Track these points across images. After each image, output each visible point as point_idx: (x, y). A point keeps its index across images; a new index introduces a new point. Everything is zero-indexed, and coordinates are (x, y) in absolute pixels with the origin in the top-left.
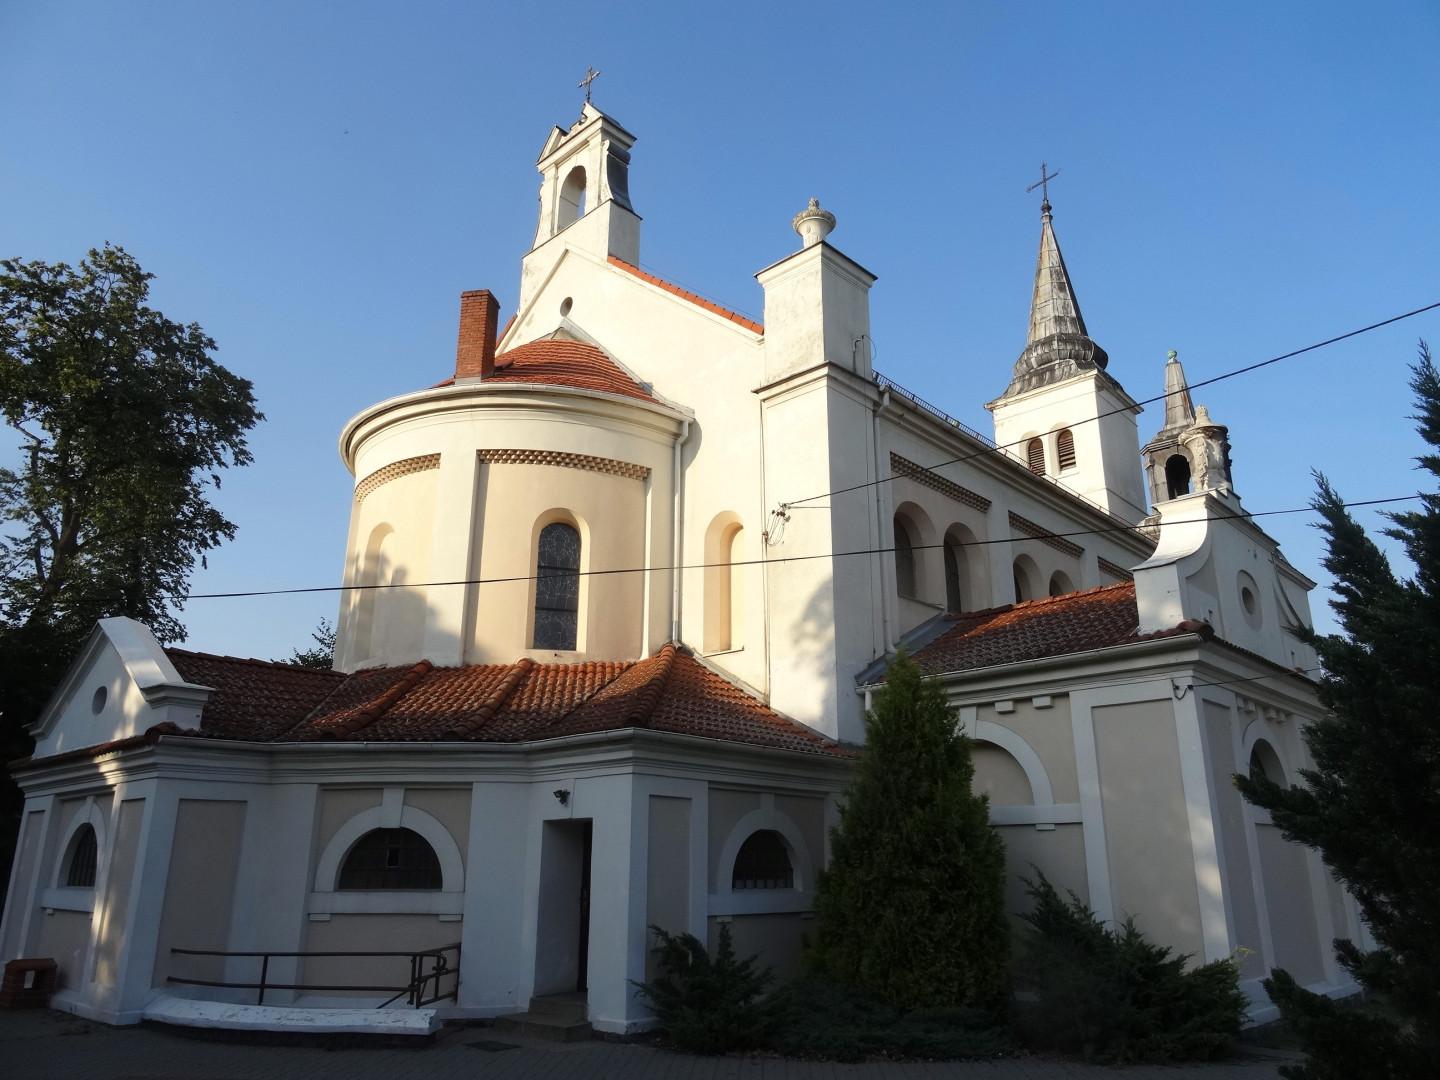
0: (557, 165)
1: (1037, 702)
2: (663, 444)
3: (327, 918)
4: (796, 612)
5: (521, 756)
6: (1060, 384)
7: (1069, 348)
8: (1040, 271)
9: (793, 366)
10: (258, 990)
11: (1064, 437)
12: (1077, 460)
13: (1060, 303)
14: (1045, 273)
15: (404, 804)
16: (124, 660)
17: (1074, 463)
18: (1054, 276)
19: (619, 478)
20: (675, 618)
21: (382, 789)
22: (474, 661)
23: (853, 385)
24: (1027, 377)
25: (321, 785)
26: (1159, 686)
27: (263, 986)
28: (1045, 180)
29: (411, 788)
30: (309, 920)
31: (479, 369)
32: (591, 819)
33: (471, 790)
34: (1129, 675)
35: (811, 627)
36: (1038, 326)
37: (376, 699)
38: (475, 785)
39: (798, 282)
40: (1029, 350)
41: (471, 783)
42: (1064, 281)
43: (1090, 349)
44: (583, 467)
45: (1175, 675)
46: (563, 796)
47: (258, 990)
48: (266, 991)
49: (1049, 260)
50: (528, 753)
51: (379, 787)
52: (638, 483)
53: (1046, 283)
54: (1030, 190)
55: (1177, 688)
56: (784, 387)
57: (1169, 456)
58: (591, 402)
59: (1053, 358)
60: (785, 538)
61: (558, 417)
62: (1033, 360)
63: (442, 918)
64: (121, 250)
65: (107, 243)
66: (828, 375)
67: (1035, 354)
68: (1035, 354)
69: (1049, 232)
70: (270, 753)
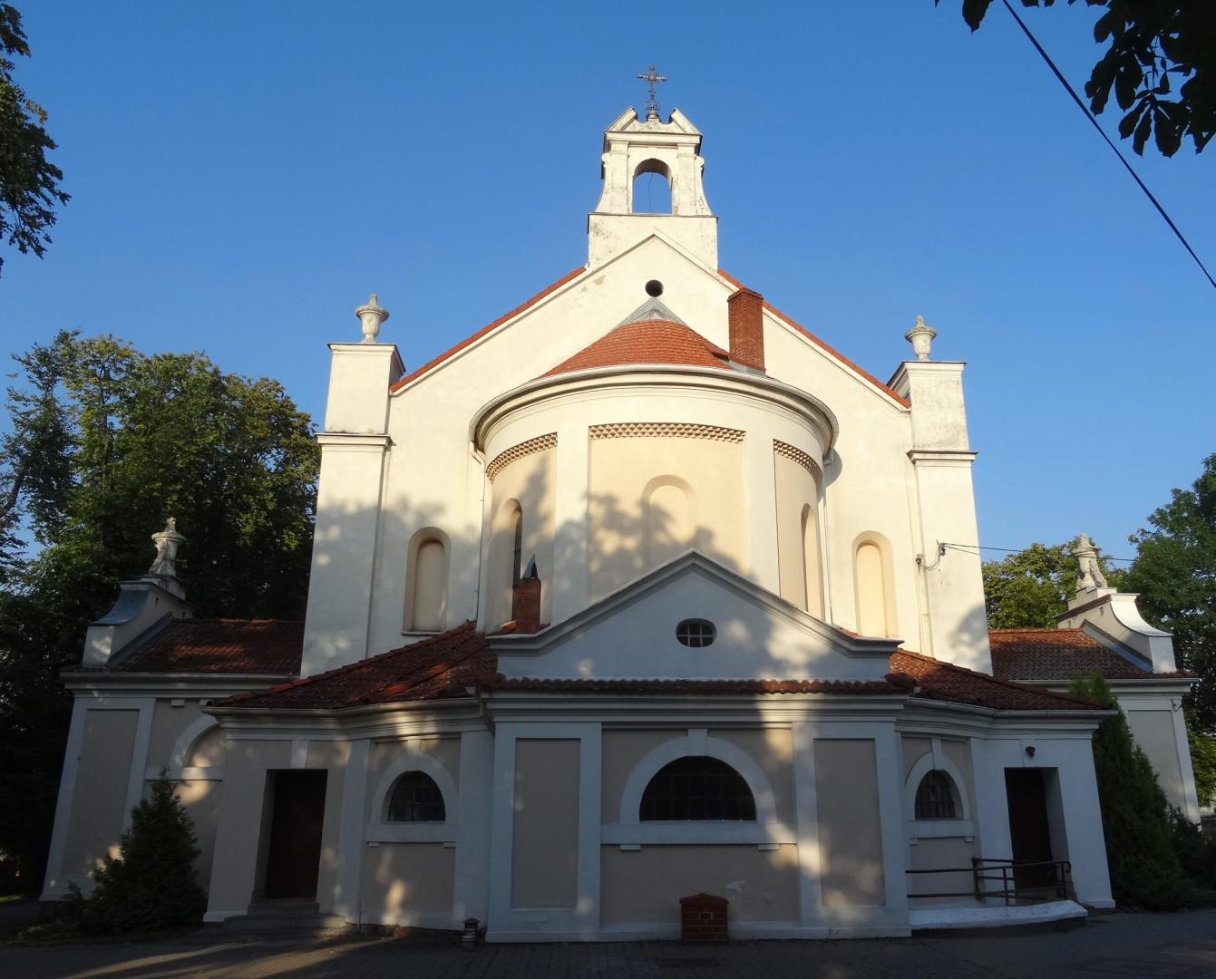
1: (174, 703)
3: (638, 848)
4: (951, 624)
5: (990, 719)
9: (941, 443)
16: (1095, 599)
21: (686, 730)
26: (1163, 703)
32: (270, 772)
33: (460, 739)
35: (965, 637)
37: (195, 645)
39: (941, 382)
41: (459, 733)
45: (1173, 698)
46: (1030, 751)
50: (994, 717)
55: (1174, 705)
56: (937, 456)
60: (940, 566)
63: (623, 848)
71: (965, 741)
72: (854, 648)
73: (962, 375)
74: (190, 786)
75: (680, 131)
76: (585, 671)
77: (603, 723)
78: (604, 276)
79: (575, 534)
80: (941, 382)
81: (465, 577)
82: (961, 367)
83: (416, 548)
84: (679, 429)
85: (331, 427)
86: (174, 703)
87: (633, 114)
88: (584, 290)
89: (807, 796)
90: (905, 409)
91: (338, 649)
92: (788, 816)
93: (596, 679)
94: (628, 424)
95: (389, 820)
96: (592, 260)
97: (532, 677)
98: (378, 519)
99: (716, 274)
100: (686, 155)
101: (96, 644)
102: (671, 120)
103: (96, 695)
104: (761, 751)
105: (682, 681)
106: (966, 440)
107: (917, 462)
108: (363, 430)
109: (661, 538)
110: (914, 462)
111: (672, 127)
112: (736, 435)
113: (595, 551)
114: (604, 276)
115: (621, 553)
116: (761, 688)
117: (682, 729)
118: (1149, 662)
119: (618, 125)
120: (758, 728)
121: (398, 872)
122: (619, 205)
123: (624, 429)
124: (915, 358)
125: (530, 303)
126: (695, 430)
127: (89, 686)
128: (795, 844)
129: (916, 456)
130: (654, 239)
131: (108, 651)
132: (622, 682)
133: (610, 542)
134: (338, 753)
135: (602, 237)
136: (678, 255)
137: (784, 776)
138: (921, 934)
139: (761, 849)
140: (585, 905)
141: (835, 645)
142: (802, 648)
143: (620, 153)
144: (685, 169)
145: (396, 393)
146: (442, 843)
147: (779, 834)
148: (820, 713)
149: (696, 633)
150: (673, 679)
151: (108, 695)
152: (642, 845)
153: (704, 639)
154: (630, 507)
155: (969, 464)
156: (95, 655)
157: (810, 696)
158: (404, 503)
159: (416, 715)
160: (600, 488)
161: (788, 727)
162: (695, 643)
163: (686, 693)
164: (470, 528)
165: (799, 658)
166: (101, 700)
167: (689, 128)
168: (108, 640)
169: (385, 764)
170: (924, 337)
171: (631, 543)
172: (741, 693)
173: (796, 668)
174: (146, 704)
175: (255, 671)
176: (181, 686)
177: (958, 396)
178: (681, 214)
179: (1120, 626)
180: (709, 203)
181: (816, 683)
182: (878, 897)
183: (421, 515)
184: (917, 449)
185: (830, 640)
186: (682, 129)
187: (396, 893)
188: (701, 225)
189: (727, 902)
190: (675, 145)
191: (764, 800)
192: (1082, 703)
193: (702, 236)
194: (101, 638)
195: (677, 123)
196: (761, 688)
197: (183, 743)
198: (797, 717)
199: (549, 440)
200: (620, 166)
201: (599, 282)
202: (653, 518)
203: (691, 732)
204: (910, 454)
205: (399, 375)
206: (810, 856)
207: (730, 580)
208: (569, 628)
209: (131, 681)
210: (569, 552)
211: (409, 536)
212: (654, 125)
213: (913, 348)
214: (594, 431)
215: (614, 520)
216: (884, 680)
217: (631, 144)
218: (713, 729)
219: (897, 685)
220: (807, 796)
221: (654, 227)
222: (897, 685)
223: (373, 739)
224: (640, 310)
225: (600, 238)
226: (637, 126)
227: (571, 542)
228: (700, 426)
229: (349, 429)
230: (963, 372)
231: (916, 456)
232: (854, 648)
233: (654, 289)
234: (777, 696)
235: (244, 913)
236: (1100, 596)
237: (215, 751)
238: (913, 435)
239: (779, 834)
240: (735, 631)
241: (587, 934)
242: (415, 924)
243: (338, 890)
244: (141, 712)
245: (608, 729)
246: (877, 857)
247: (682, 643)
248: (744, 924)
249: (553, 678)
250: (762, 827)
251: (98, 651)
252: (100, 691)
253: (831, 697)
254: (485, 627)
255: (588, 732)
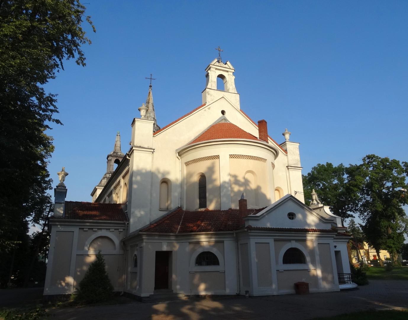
3: (283, 271)
9: (294, 164)
33: (224, 242)
56: (294, 168)
63: (280, 271)
71: (223, 242)
72: (325, 221)
73: (299, 146)
74: (90, 257)
75: (228, 67)
76: (268, 225)
77: (274, 239)
78: (210, 107)
79: (226, 185)
80: (294, 148)
81: (175, 194)
82: (298, 144)
83: (161, 183)
84: (253, 158)
85: (136, 145)
86: (85, 230)
87: (217, 60)
88: (205, 110)
89: (317, 258)
90: (286, 154)
91: (141, 215)
92: (314, 263)
93: (270, 227)
94: (240, 155)
95: (196, 265)
96: (207, 102)
97: (258, 227)
98: (151, 175)
99: (239, 111)
100: (231, 75)
101: (58, 210)
102: (226, 64)
103: (59, 226)
104: (306, 246)
105: (290, 228)
106: (300, 164)
107: (289, 169)
108: (146, 146)
109: (248, 188)
110: (288, 169)
111: (226, 66)
112: (265, 160)
113: (232, 191)
114: (210, 107)
115: (239, 191)
116: (307, 231)
117: (289, 240)
118: (336, 224)
119: (213, 63)
120: (305, 240)
121: (202, 280)
122: (214, 87)
123: (239, 156)
124: (140, 117)
125: (191, 113)
126: (256, 158)
127: (57, 223)
128: (315, 269)
129: (289, 167)
130: (223, 98)
131: (62, 212)
132: (278, 228)
133: (236, 188)
134: (174, 246)
135: (210, 96)
136: (229, 104)
137: (312, 252)
138: (342, 290)
139: (308, 270)
140: (274, 286)
141: (320, 220)
142: (313, 221)
143: (213, 71)
144: (230, 79)
145: (155, 136)
146: (219, 271)
147: (311, 267)
148: (319, 237)
149: (291, 216)
150: (289, 228)
151: (63, 227)
152: (284, 270)
153: (292, 218)
154: (241, 179)
155: (301, 170)
156: (58, 213)
157: (318, 233)
158: (158, 170)
159: (206, 236)
160: (233, 173)
161: (312, 241)
162: (290, 218)
163: (293, 231)
164: (177, 180)
165: (313, 224)
166: (60, 228)
167: (231, 67)
168: (62, 208)
169: (193, 251)
170: (144, 110)
171: (242, 189)
172: (274, 231)
173: (312, 226)
174: (76, 230)
175: (109, 220)
176: (88, 224)
177: (298, 152)
178: (230, 92)
179: (326, 214)
180: (236, 90)
181: (318, 229)
182: (333, 282)
183: (163, 174)
184: (289, 165)
185: (318, 218)
186: (230, 67)
187: (202, 287)
188: (235, 96)
189: (294, 284)
190: (228, 71)
191: (308, 259)
192: (345, 235)
193: (236, 99)
194: (59, 208)
195: (228, 65)
196: (307, 231)
197: (88, 243)
198: (314, 238)
199: (217, 157)
200: (213, 75)
201: (209, 109)
202: (246, 183)
203: (292, 241)
204: (287, 167)
205: (157, 130)
206: (319, 273)
207: (300, 204)
208: (265, 214)
209: (65, 222)
210: (225, 190)
211: (160, 181)
212: (222, 64)
213: (140, 113)
214: (230, 156)
215: (237, 182)
216: (330, 229)
217: (216, 69)
218: (297, 240)
219: (334, 230)
220: (317, 258)
221: (224, 95)
222: (334, 230)
223: (189, 242)
224: (220, 118)
225: (209, 96)
226: (217, 64)
227: (225, 187)
228: (258, 157)
229: (142, 146)
230: (299, 146)
231: (289, 167)
232: (325, 221)
233: (223, 112)
234: (311, 233)
235: (153, 294)
236: (319, 206)
237: (96, 246)
238: (288, 162)
239: (311, 267)
240: (299, 216)
241: (275, 293)
242: (213, 294)
243: (178, 287)
244: (75, 233)
245: (275, 240)
246: (332, 273)
247: (289, 218)
248: (312, 289)
249: (263, 227)
250: (308, 265)
251: (59, 212)
252: (61, 225)
253: (322, 233)
254: (186, 209)
255: (271, 241)
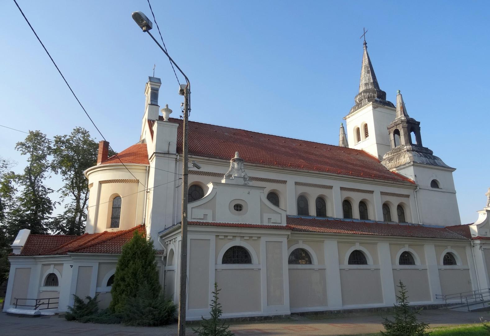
0: (147, 93)
2: (144, 173)
6: (364, 107)
7: (367, 94)
8: (362, 67)
10: (17, 304)
11: (366, 126)
12: (369, 135)
13: (367, 78)
14: (363, 67)
15: (54, 268)
17: (368, 136)
18: (366, 68)
19: (131, 183)
20: (144, 217)
22: (97, 232)
23: (165, 156)
24: (355, 107)
25: (42, 264)
27: (16, 305)
28: (365, 33)
29: (55, 265)
30: (39, 292)
31: (101, 161)
33: (63, 265)
34: (177, 234)
36: (360, 87)
38: (64, 264)
40: (356, 97)
41: (63, 263)
42: (371, 69)
43: (375, 93)
44: (122, 182)
47: (48, 304)
48: (48, 303)
49: (366, 62)
51: (50, 265)
52: (136, 184)
53: (363, 72)
54: (361, 38)
57: (394, 130)
58: (120, 166)
59: (363, 98)
61: (115, 171)
62: (357, 100)
64: (80, 127)
65: (76, 127)
66: (155, 156)
67: (357, 98)
68: (357, 98)
69: (365, 52)
70: (35, 258)
